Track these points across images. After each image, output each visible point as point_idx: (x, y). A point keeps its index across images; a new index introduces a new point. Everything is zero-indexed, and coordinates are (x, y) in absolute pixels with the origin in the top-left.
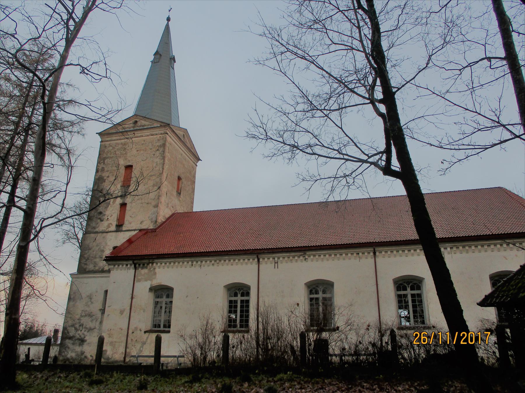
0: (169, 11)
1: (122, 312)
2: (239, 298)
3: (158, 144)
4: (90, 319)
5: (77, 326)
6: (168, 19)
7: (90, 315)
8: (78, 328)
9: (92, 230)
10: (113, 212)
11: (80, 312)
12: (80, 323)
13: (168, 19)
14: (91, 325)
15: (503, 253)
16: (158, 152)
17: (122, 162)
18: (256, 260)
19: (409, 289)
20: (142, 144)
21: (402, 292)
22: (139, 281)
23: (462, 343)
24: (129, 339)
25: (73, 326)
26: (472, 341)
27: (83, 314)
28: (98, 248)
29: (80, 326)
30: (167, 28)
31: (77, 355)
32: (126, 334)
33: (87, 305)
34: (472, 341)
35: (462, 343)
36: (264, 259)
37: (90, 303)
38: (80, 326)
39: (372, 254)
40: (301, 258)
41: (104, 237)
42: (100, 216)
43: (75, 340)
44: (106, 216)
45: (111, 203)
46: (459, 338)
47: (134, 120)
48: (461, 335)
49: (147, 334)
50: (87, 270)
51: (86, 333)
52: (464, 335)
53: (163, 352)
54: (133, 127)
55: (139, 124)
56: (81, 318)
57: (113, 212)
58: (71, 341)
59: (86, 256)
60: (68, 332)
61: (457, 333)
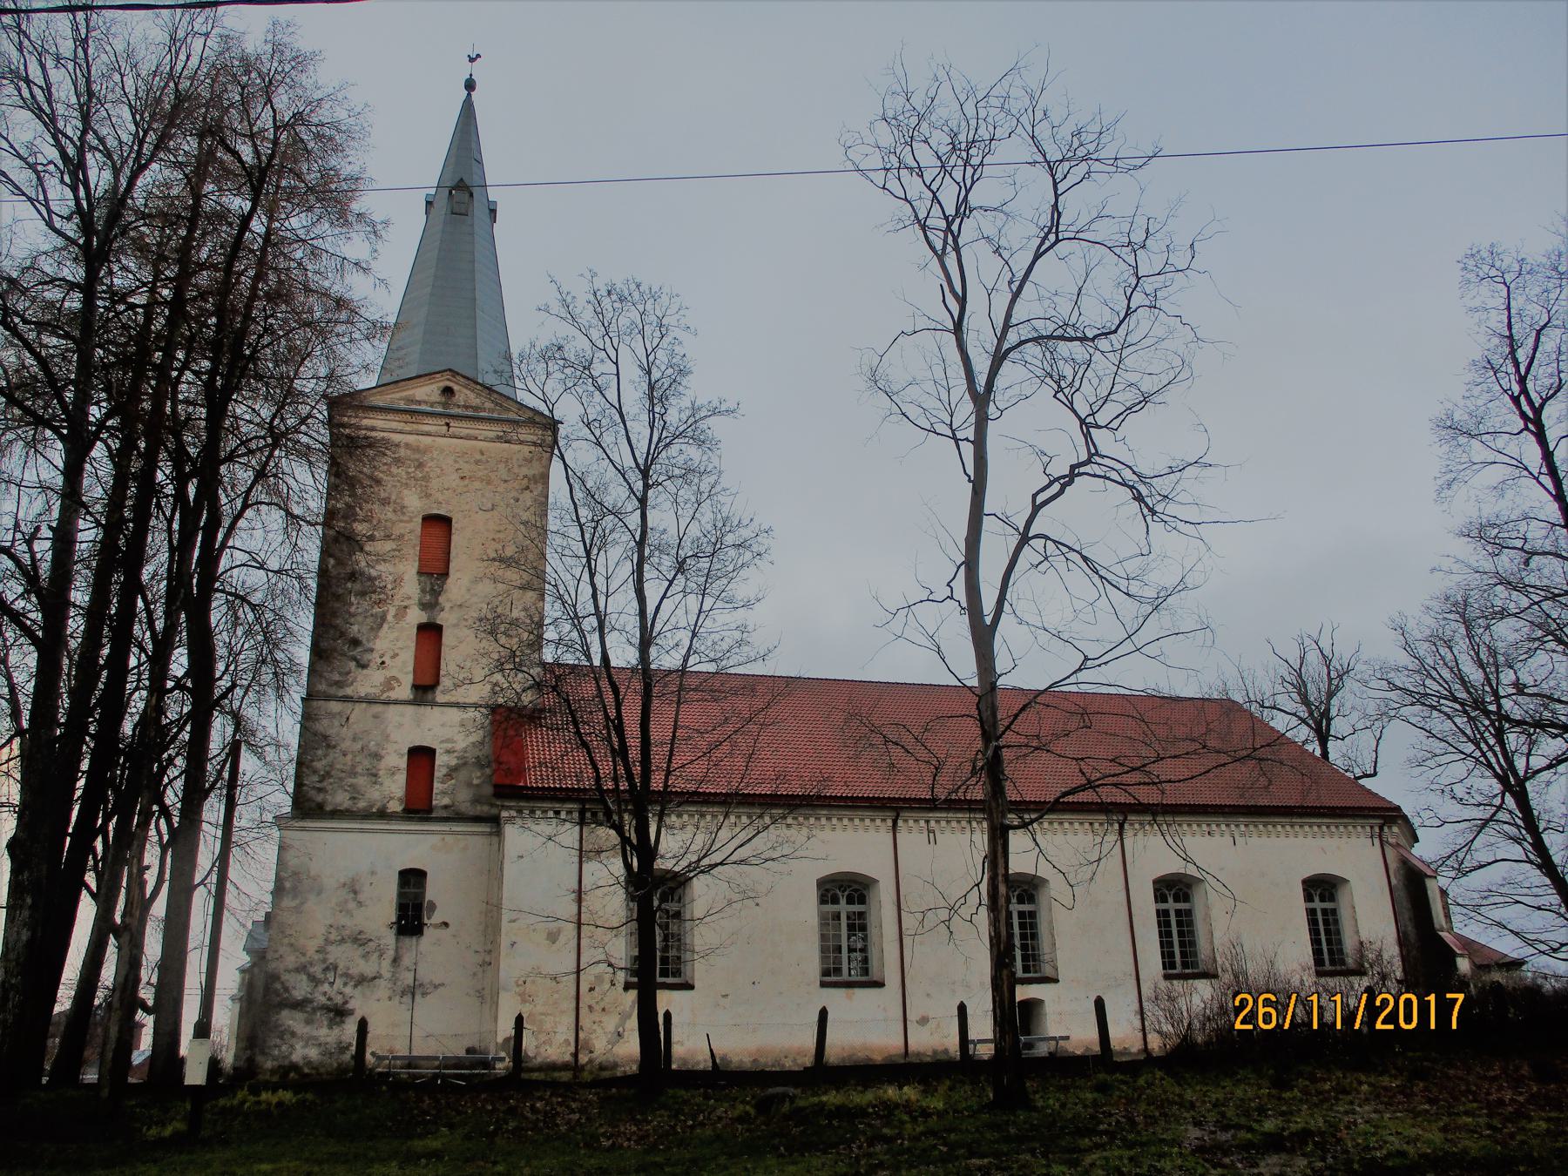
0: (472, 60)
1: (553, 937)
3: (525, 471)
4: (360, 951)
5: (317, 970)
6: (470, 85)
7: (359, 940)
8: (320, 976)
9: (333, 691)
10: (400, 644)
11: (323, 930)
12: (324, 961)
13: (470, 85)
14: (368, 968)
15: (1319, 842)
16: (527, 494)
17: (416, 504)
19: (843, 901)
20: (477, 462)
23: (1379, 1026)
25: (301, 969)
26: (1408, 1020)
27: (332, 937)
28: (358, 746)
29: (326, 969)
30: (468, 110)
31: (327, 1053)
32: (573, 993)
33: (342, 908)
34: (1408, 1020)
35: (1379, 1026)
36: (906, 821)
37: (352, 905)
38: (326, 969)
41: (375, 717)
42: (356, 652)
43: (314, 1010)
44: (375, 655)
45: (390, 617)
47: (442, 384)
50: (328, 808)
51: (348, 990)
53: (972, 1035)
54: (445, 405)
56: (330, 948)
57: (400, 644)
58: (299, 1015)
59: (318, 765)
60: (286, 990)
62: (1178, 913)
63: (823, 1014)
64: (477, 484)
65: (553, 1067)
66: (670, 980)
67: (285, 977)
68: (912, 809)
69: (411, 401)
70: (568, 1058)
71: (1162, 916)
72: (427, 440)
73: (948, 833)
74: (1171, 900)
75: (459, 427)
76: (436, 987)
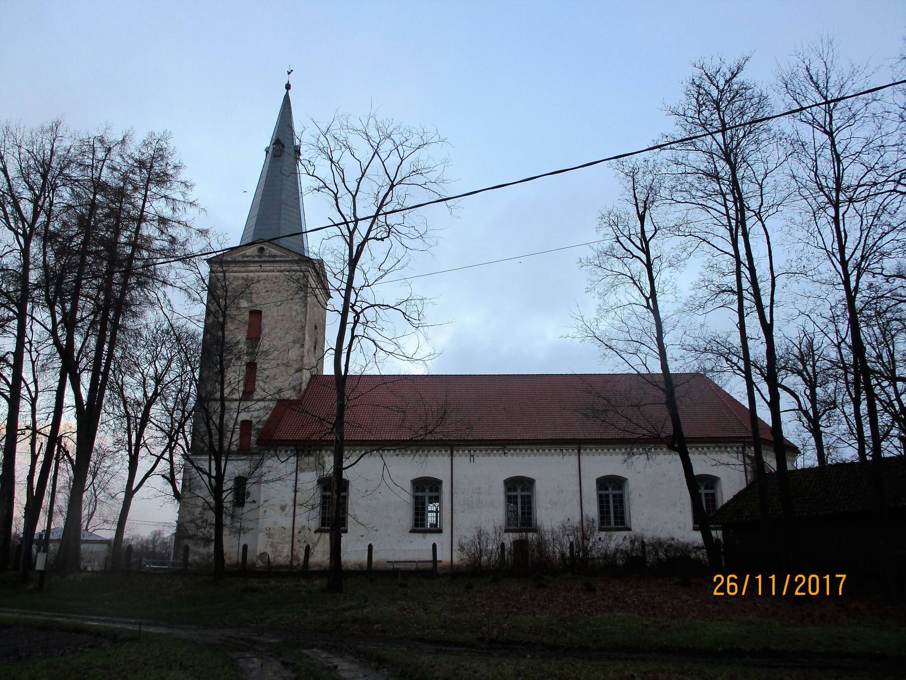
0: (289, 73)
1: (283, 508)
2: (611, 492)
6: (288, 87)
13: (288, 87)
16: (297, 296)
18: (449, 452)
20: (274, 283)
21: (419, 494)
22: (303, 471)
23: (797, 593)
24: (296, 540)
25: (192, 521)
26: (814, 590)
30: (287, 101)
34: (814, 590)
35: (797, 593)
39: (576, 451)
40: (501, 452)
46: (793, 585)
48: (796, 580)
49: (318, 534)
52: (800, 580)
54: (259, 257)
55: (267, 252)
60: (186, 530)
61: (788, 576)
62: (614, 496)
63: (434, 546)
64: (274, 294)
65: (281, 566)
66: (420, 528)
67: (186, 525)
68: (459, 445)
69: (244, 256)
70: (288, 563)
71: (600, 497)
72: (251, 274)
73: (389, 456)
74: (427, 490)
75: (267, 267)
76: (250, 530)
